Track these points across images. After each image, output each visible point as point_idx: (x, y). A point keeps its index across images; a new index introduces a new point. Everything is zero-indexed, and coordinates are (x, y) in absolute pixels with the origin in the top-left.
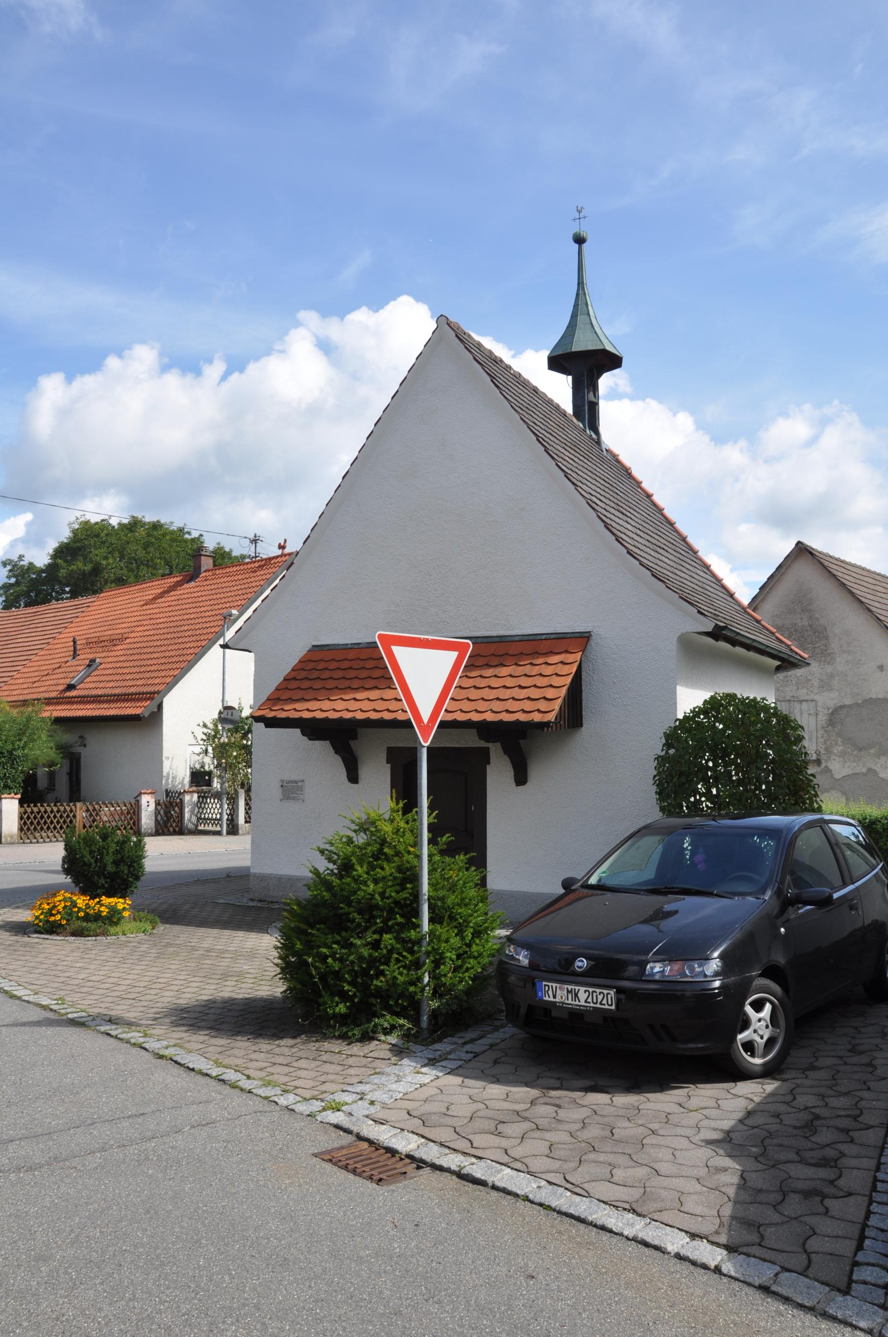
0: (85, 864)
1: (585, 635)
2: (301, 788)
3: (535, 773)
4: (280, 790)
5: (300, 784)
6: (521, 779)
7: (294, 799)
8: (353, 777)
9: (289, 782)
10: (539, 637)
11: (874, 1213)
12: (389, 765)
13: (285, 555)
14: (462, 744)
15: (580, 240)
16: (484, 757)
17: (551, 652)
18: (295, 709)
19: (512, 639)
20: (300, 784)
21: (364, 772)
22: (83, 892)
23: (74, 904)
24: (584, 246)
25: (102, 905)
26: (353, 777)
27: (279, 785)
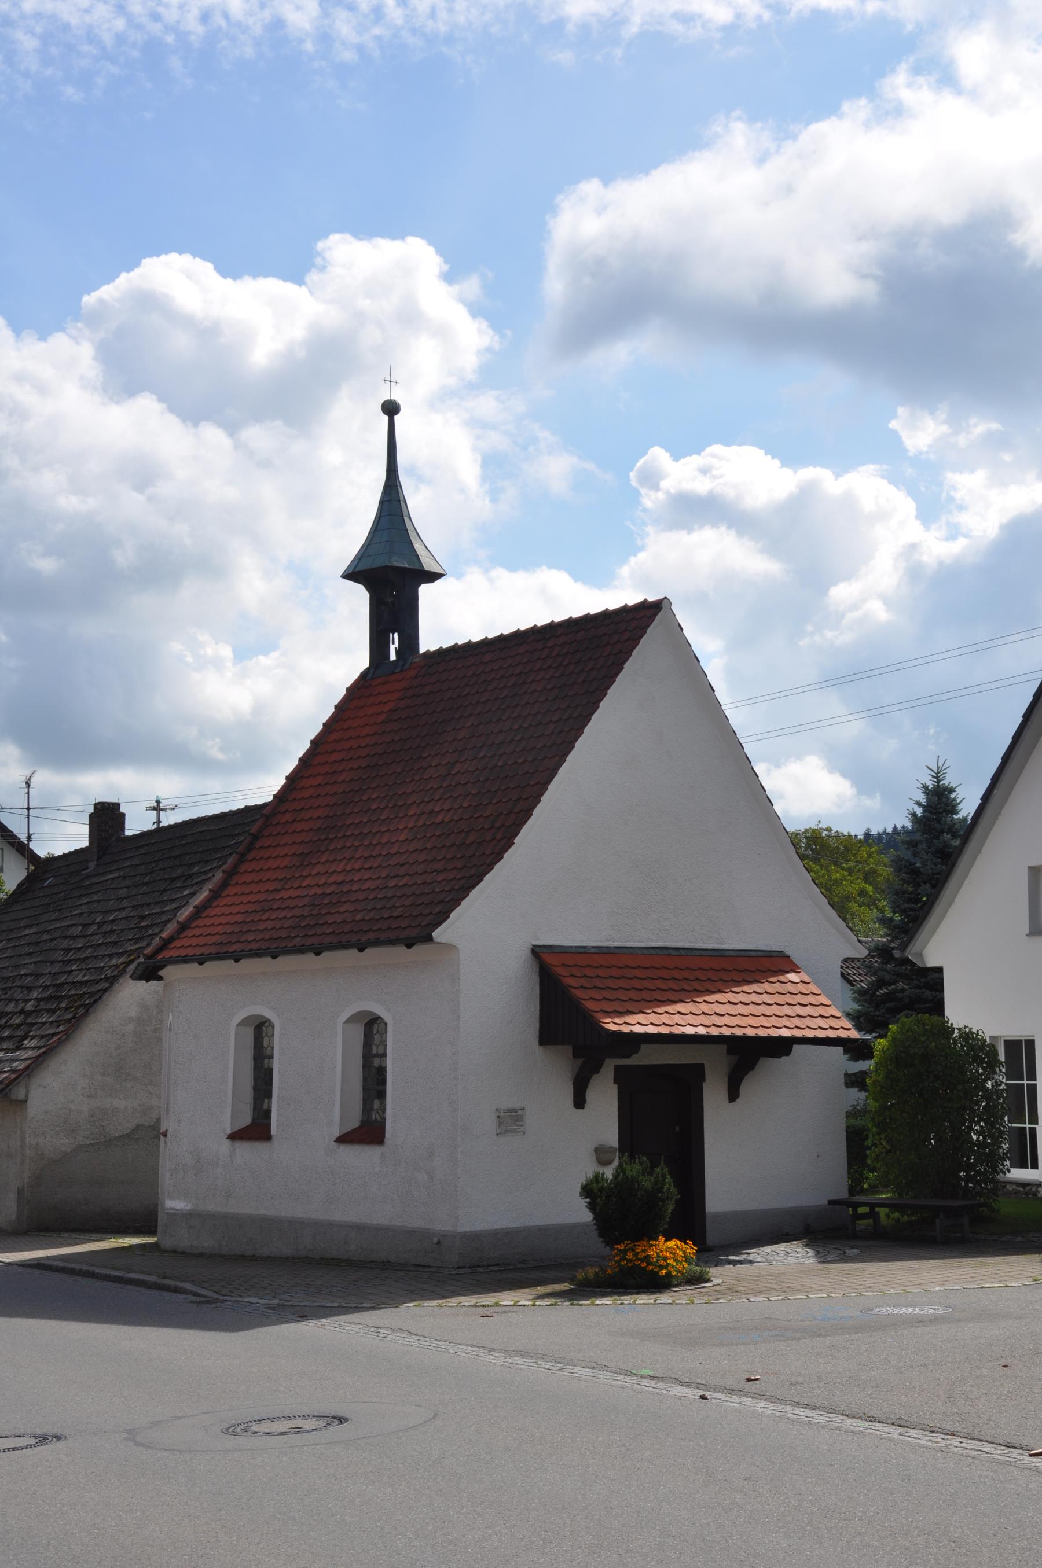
3: (746, 1088)
5: (520, 1112)
6: (733, 1095)
7: (513, 1132)
8: (579, 1102)
15: (391, 409)
16: (697, 1073)
20: (520, 1112)
21: (591, 1095)
24: (396, 417)
26: (579, 1102)
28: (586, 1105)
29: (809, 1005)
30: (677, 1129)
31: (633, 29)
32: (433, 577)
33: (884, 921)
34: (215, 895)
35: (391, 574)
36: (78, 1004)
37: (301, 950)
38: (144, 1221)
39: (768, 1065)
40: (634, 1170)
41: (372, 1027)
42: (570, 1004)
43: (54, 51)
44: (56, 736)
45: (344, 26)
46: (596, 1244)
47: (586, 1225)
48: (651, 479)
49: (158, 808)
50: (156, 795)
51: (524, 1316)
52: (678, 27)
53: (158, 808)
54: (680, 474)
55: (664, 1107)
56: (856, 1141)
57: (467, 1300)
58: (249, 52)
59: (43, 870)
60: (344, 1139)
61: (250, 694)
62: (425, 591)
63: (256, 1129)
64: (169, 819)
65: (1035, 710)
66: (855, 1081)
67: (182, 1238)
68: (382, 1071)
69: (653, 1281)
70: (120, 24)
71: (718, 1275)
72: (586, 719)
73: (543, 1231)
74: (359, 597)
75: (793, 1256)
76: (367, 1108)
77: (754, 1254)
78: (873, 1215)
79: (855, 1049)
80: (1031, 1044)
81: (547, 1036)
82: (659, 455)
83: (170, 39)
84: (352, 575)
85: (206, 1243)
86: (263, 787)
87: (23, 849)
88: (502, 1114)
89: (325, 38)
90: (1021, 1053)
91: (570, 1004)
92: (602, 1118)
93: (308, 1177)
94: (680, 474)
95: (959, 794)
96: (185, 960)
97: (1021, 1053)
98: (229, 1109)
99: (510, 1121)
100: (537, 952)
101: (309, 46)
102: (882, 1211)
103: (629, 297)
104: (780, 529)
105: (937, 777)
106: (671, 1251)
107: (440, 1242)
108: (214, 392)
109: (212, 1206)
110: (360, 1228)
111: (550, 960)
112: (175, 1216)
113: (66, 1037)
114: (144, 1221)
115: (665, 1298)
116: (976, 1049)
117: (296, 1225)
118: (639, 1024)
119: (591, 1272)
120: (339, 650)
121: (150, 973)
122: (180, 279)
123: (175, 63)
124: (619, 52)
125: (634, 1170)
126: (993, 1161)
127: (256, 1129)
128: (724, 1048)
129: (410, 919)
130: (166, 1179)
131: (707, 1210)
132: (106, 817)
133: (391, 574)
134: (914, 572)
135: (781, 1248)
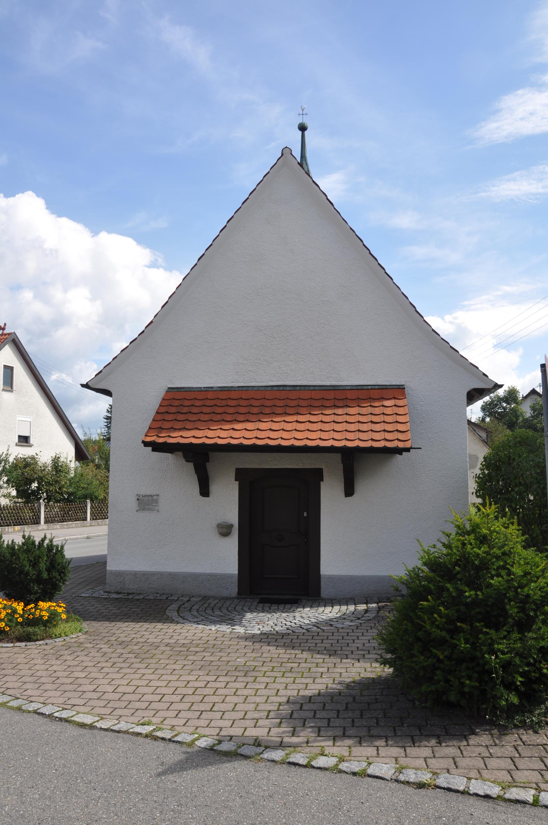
0: (21, 572)
1: (401, 387)
2: (157, 501)
3: (360, 487)
4: (137, 502)
5: (155, 497)
6: (349, 491)
7: (149, 509)
8: (205, 492)
9: (145, 496)
10: (366, 387)
11: (405, 750)
12: (237, 482)
13: (5, 335)
14: (301, 466)
15: (303, 128)
16: (317, 475)
17: (382, 398)
18: (181, 436)
19: (344, 388)
20: (155, 497)
21: (214, 488)
22: (18, 599)
23: (14, 611)
24: (306, 132)
25: (41, 610)
26: (205, 492)
27: (135, 499)
28: (210, 495)
30: (305, 515)
47: (230, 576)
88: (141, 498)
128: (338, 457)
131: (322, 573)
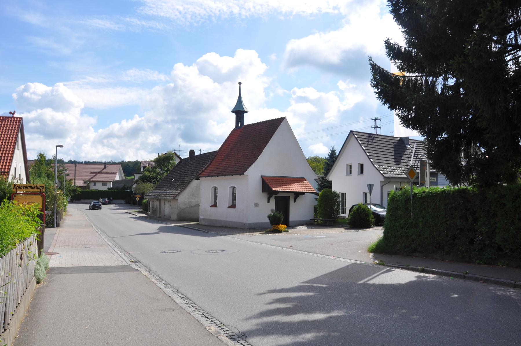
3: (297, 200)
6: (295, 201)
8: (269, 202)
15: (240, 84)
16: (289, 197)
21: (270, 201)
26: (269, 202)
29: (309, 187)
31: (294, 13)
32: (246, 112)
33: (323, 173)
34: (209, 166)
35: (239, 112)
36: (186, 184)
37: (222, 175)
38: (197, 220)
39: (301, 197)
40: (276, 213)
41: (215, 188)
42: (267, 186)
43: (193, 17)
44: (188, 137)
45: (243, 12)
46: (270, 225)
48: (294, 93)
49: (200, 151)
50: (203, 148)
51: (257, 236)
52: (302, 13)
53: (200, 151)
54: (300, 92)
55: (283, 203)
56: (315, 209)
57: (248, 234)
58: (226, 17)
59: (182, 160)
60: (229, 207)
61: (215, 133)
62: (245, 114)
63: (215, 205)
64: (202, 153)
65: (91, 161)
66: (316, 199)
67: (202, 222)
68: (235, 196)
69: (279, 231)
70: (205, 12)
71: (290, 231)
72: (271, 137)
73: (262, 223)
74: (234, 115)
75: (304, 228)
76: (233, 202)
77: (297, 228)
78: (317, 221)
79: (317, 194)
80: (345, 194)
81: (263, 191)
82: (296, 89)
83: (213, 15)
84: (232, 112)
85: (206, 223)
86: (216, 147)
87: (178, 157)
89: (240, 14)
90: (344, 195)
91: (267, 186)
92: (272, 205)
93: (223, 213)
94: (300, 92)
95: (336, 151)
96: (203, 177)
97: (344, 195)
98: (211, 202)
99: (256, 205)
100: (262, 177)
101: (237, 16)
102: (319, 221)
103: (300, 60)
104: (316, 103)
105: (333, 148)
106: (282, 227)
107: (244, 224)
108: (219, 78)
109: (207, 218)
110: (231, 222)
111: (264, 178)
112: (201, 219)
113: (184, 189)
114: (197, 220)
115: (281, 234)
116: (336, 195)
117: (221, 221)
118: (279, 189)
119: (269, 230)
120: (229, 124)
121: (198, 179)
122: (212, 58)
123: (213, 19)
124: (291, 17)
125: (276, 213)
126: (338, 213)
127: (215, 205)
129: (240, 170)
130: (200, 213)
132: (192, 152)
133: (239, 112)
134: (339, 111)
135: (302, 227)
